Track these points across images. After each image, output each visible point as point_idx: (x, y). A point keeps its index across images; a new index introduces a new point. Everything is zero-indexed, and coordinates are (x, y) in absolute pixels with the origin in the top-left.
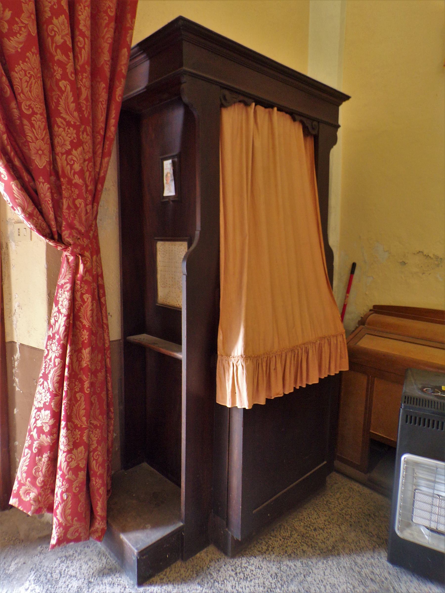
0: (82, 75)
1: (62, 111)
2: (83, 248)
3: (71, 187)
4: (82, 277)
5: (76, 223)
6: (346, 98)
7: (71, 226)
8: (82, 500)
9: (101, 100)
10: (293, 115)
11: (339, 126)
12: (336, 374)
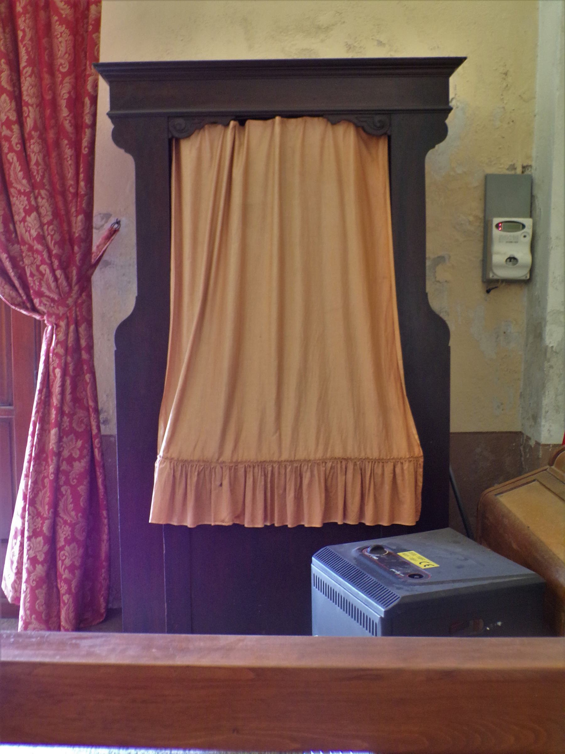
0: (30, 142)
1: (13, 181)
2: (58, 318)
3: (33, 254)
5: (44, 289)
6: (454, 63)
7: (40, 294)
8: (40, 597)
9: (66, 156)
10: (333, 117)
12: (266, 526)
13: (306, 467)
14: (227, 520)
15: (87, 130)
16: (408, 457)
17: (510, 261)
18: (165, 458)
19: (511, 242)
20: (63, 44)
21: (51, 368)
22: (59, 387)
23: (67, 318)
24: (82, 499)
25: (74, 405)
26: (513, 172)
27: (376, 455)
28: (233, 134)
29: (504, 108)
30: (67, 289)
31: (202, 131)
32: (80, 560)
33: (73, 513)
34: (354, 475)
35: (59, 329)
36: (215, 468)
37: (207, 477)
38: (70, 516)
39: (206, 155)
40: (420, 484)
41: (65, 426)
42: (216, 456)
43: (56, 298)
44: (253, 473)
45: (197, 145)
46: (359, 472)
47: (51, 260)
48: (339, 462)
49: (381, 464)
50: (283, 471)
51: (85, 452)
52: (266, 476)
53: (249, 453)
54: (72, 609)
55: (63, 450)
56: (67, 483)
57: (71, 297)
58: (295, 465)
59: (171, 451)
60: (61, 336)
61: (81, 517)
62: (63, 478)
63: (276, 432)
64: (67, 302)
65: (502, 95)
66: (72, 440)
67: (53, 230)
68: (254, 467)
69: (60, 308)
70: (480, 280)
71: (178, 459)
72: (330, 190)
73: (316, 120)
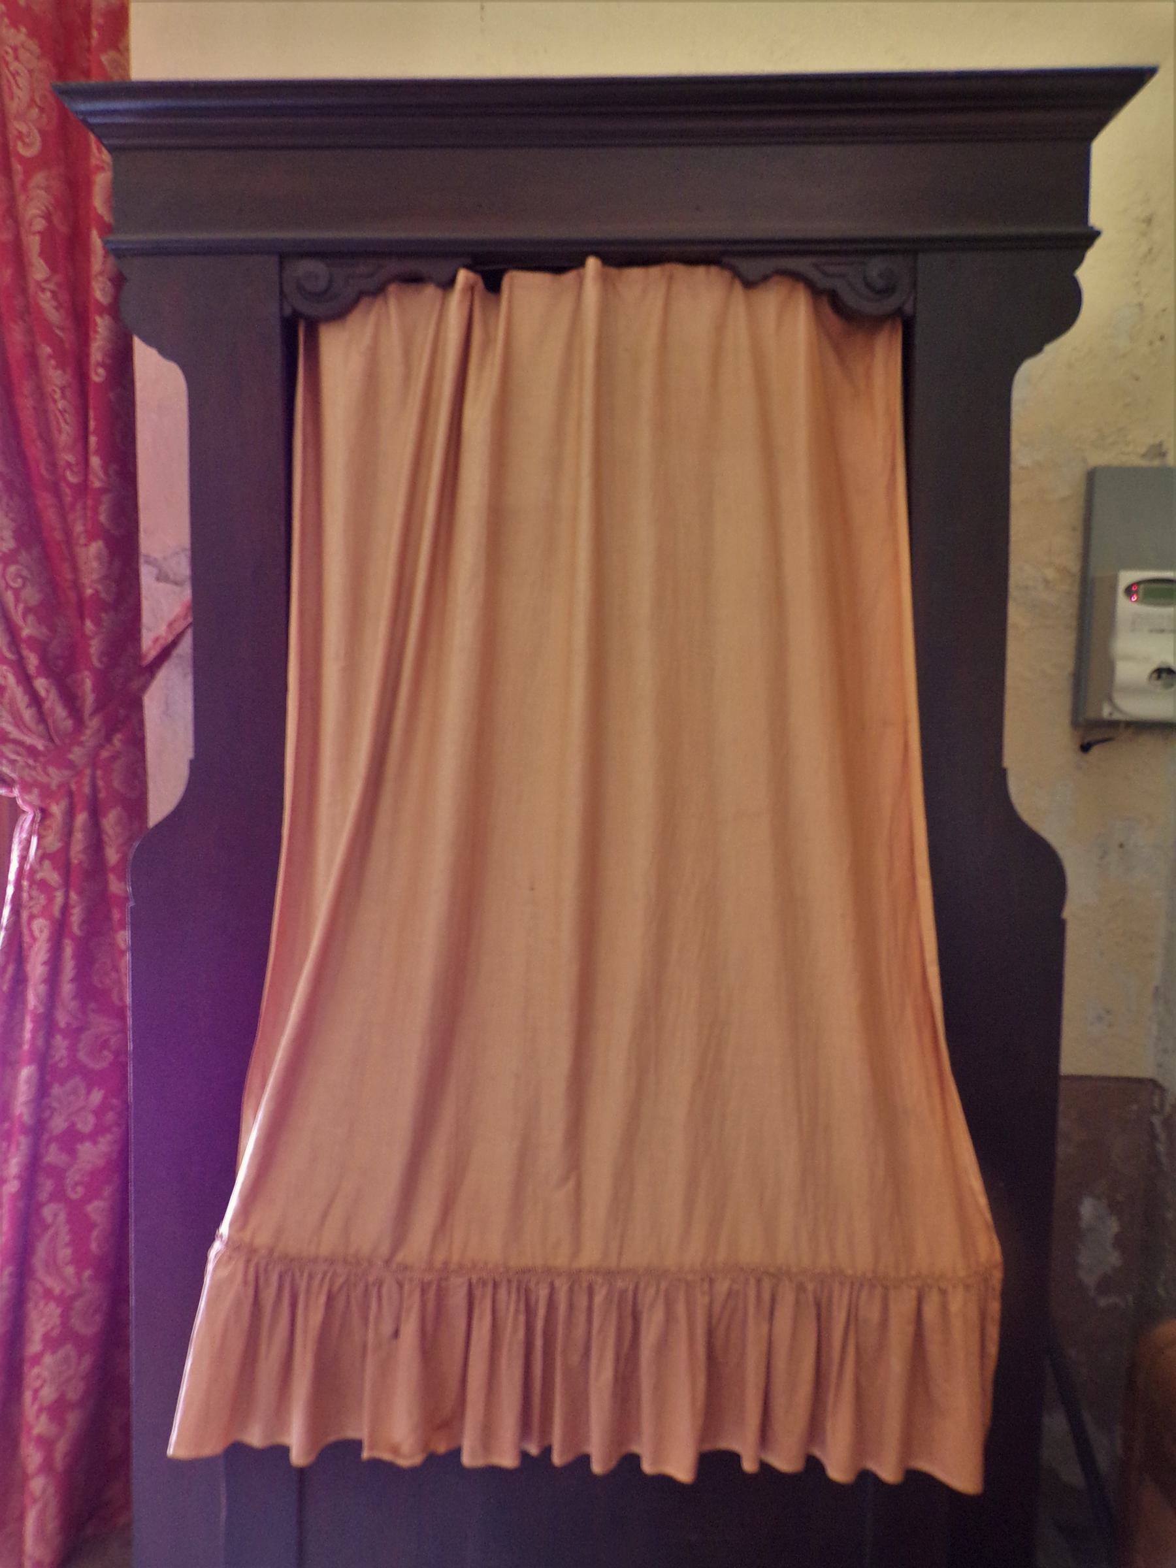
2: (46, 793)
4: (33, 872)
6: (1105, 92)
10: (741, 259)
11: (1092, 236)
13: (652, 1291)
14: (406, 1448)
15: (98, 319)
16: (962, 1273)
17: (1159, 677)
18: (234, 1246)
19: (1162, 631)
20: (23, 81)
21: (25, 915)
22: (45, 963)
23: (71, 795)
24: (95, 1233)
25: (83, 1009)
26: (1156, 463)
27: (863, 1261)
28: (467, 304)
29: (1140, 305)
30: (68, 724)
31: (379, 301)
32: (81, 1386)
33: (70, 1271)
34: (795, 1321)
35: (48, 822)
36: (380, 1284)
37: (355, 1308)
38: (64, 1279)
39: (392, 371)
40: (993, 1349)
41: (57, 1058)
42: (384, 1249)
43: (40, 747)
44: (494, 1301)
45: (367, 340)
46: (813, 1311)
47: (18, 653)
48: (752, 1281)
49: (879, 1291)
50: (582, 1302)
51: (110, 1117)
52: (530, 1312)
53: (483, 1241)
54: (52, 1509)
55: (52, 1114)
56: (58, 1195)
57: (81, 744)
58: (620, 1284)
59: (253, 1222)
60: (53, 842)
61: (91, 1279)
62: (47, 1186)
63: (565, 1179)
64: (71, 756)
65: (1137, 274)
66: (74, 1091)
67: (18, 575)
68: (496, 1286)
69: (52, 770)
70: (1065, 720)
71: (271, 1251)
72: (739, 472)
73: (700, 272)
